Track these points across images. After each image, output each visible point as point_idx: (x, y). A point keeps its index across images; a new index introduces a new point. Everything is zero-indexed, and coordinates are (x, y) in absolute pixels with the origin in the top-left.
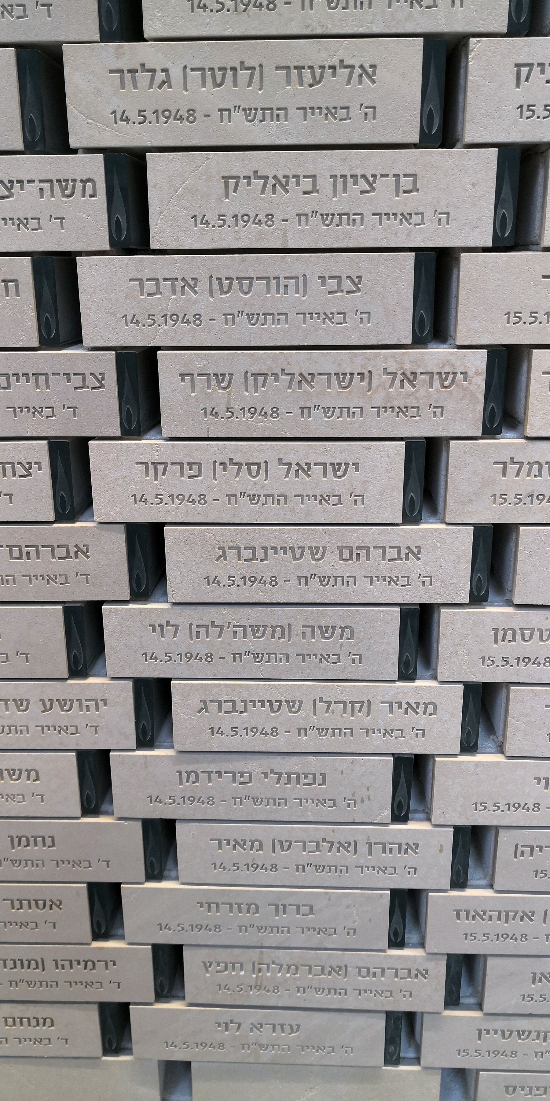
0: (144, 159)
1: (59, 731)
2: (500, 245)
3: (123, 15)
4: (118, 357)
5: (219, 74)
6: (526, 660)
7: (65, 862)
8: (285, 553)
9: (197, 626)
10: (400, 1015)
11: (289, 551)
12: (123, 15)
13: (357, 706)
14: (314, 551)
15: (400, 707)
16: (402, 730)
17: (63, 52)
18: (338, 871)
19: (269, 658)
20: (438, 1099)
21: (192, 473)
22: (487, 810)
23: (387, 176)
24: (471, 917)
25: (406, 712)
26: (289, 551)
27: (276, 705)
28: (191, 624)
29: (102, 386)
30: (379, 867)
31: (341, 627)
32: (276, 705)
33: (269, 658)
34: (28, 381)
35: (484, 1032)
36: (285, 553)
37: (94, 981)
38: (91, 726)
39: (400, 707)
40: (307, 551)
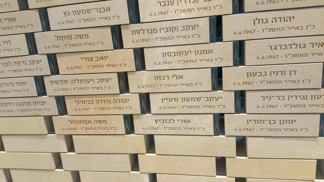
1: (209, 107)
2: (237, 111)
4: (123, 116)
6: (270, 106)
9: (72, 80)
10: (52, 54)
15: (316, 45)
16: (222, 59)
17: (315, 174)
19: (274, 130)
21: (5, 105)
23: (267, 120)
24: (186, 122)
25: (319, 47)
26: (168, 99)
27: (171, 99)
28: (71, 80)
32: (171, 99)
33: (274, 130)
34: (167, 100)
39: (316, 45)
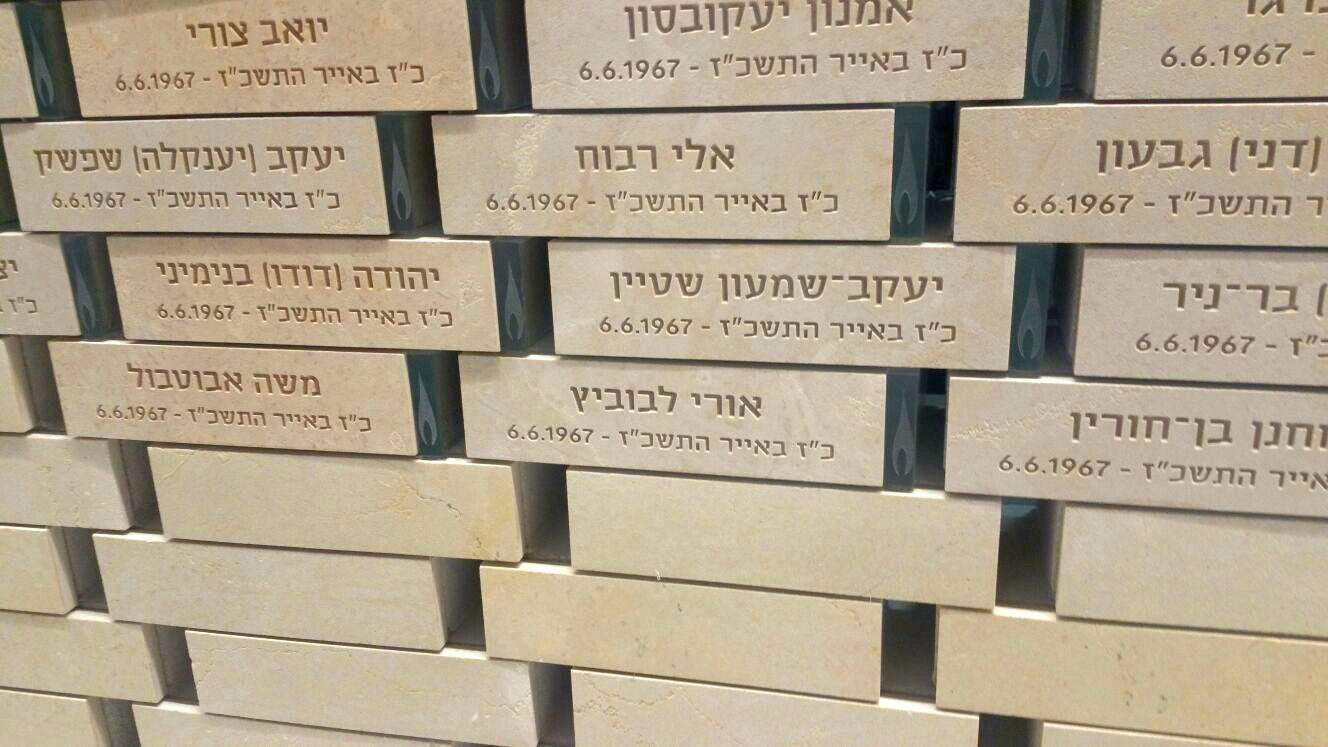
0: (502, 345)
3: (1063, 60)
5: (183, 377)
7: (856, 327)
8: (643, 283)
11: (649, 280)
12: (1063, 60)
13: (887, 285)
14: (684, 281)
18: (1236, 479)
20: (975, 743)
22: (1179, 350)
26: (649, 280)
29: (245, 42)
30: (872, 326)
31: (774, 277)
35: (1085, 421)
36: (643, 283)
37: (886, 324)
38: (746, 322)
40: (675, 280)
